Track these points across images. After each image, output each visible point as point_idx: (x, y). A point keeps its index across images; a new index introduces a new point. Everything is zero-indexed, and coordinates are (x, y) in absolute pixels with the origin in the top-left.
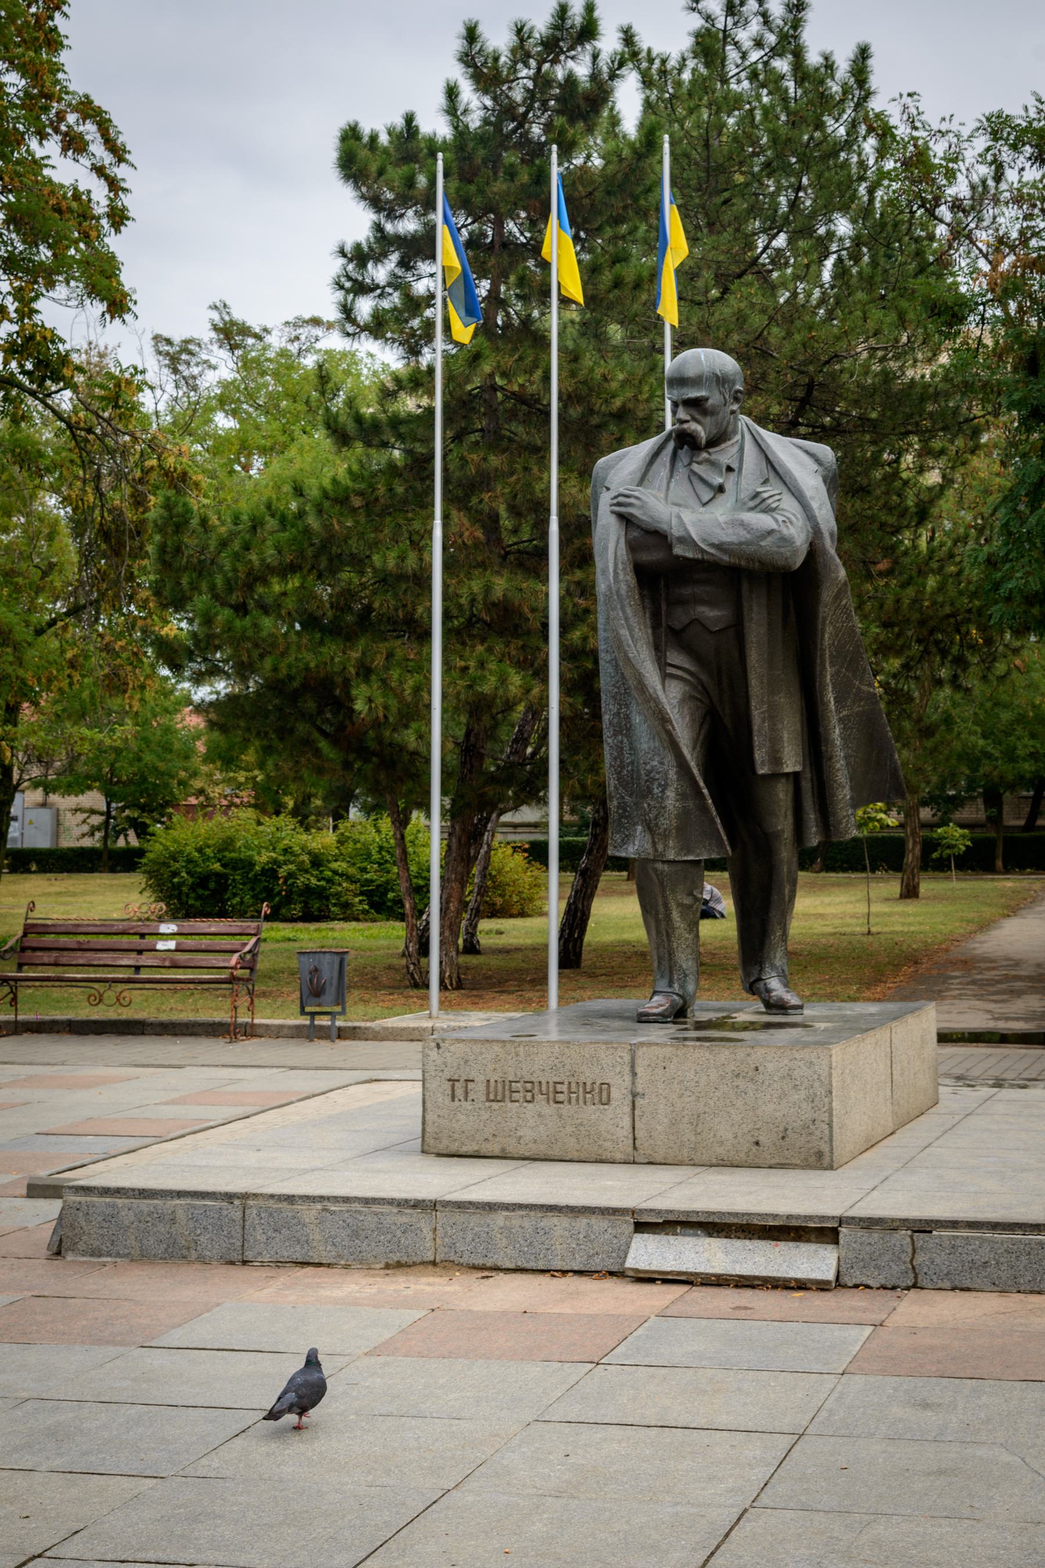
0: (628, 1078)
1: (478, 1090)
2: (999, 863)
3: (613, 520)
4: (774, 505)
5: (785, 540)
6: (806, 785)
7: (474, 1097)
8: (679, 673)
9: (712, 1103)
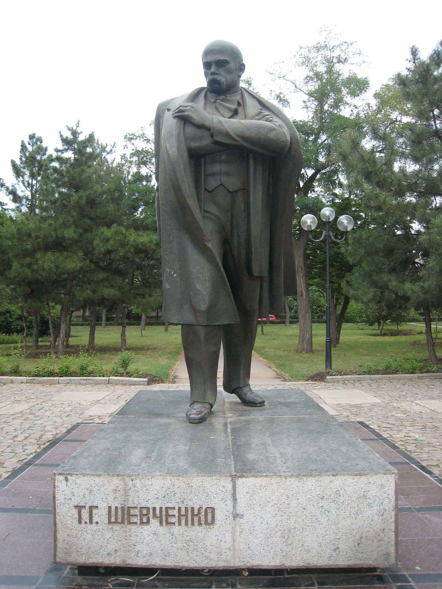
0: (230, 504)
1: (101, 515)
7: (98, 520)
8: (213, 217)
9: (300, 520)
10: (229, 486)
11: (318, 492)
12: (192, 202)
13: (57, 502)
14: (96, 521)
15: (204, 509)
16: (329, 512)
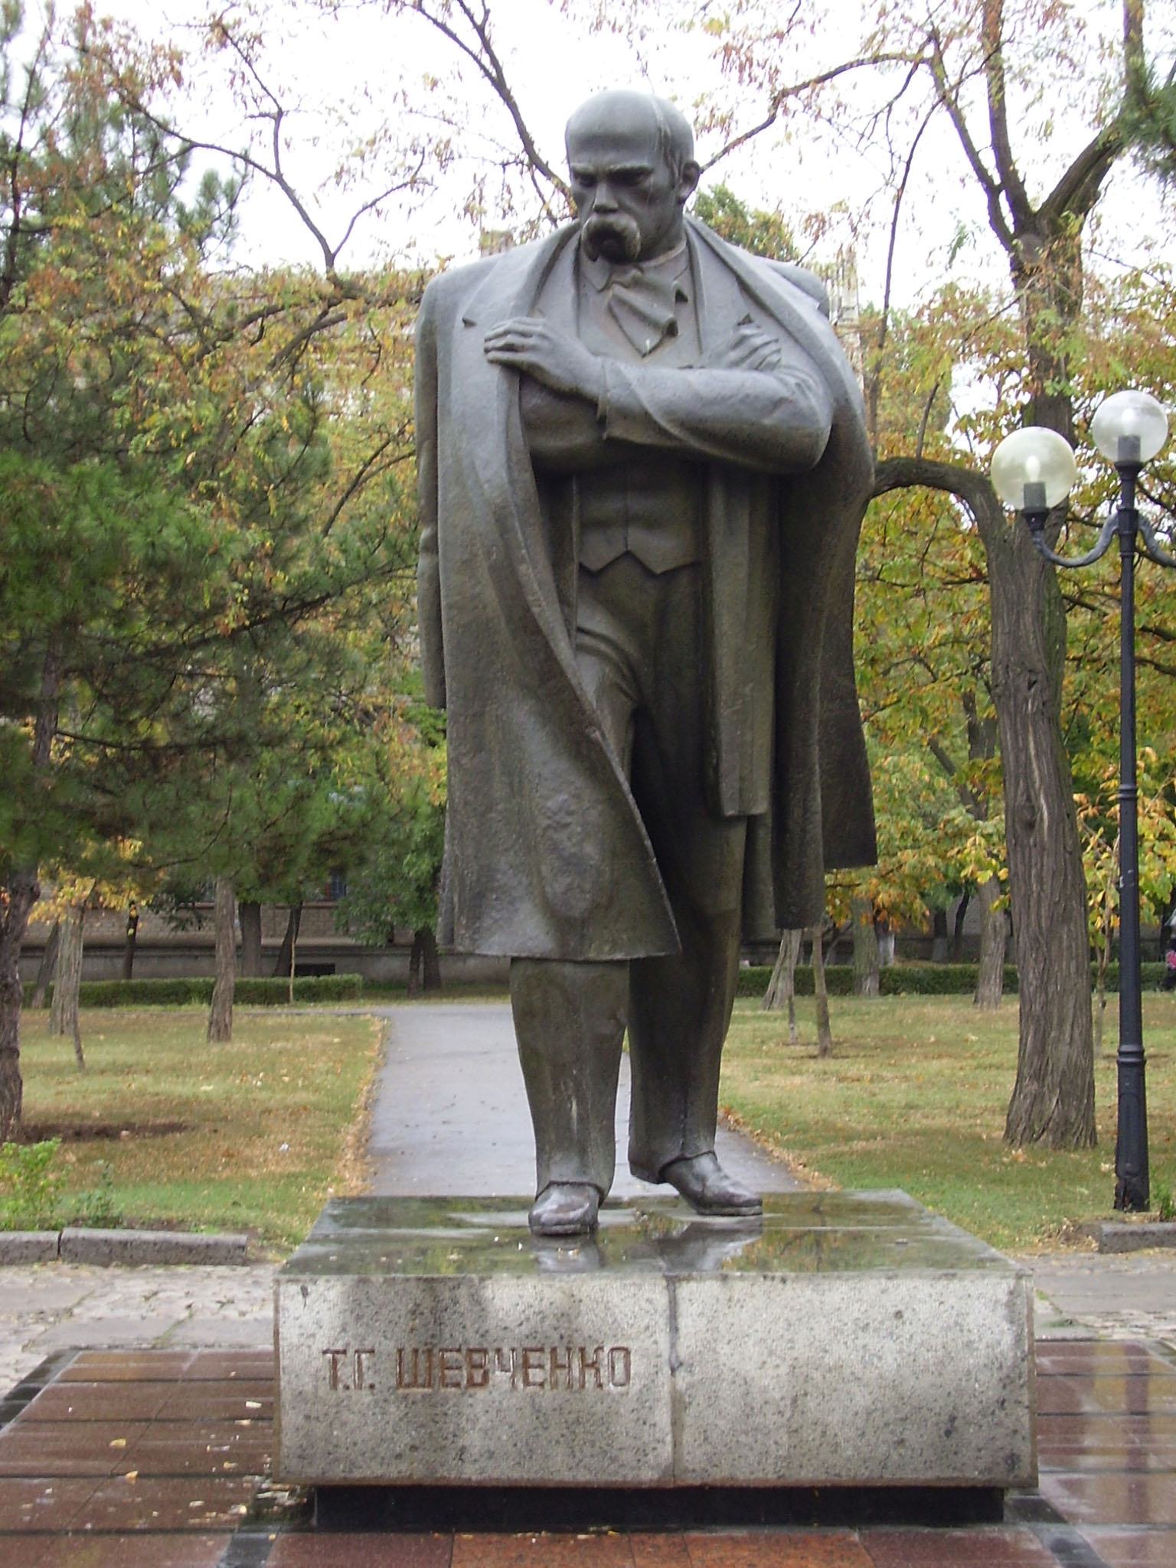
2: (974, 967)
3: (493, 378)
4: (774, 358)
5: (807, 416)
6: (764, 838)
8: (603, 647)
10: (661, 1299)
11: (856, 1315)
12: (548, 613)
13: (281, 1343)
14: (370, 1382)
15: (607, 1349)
16: (880, 1358)
